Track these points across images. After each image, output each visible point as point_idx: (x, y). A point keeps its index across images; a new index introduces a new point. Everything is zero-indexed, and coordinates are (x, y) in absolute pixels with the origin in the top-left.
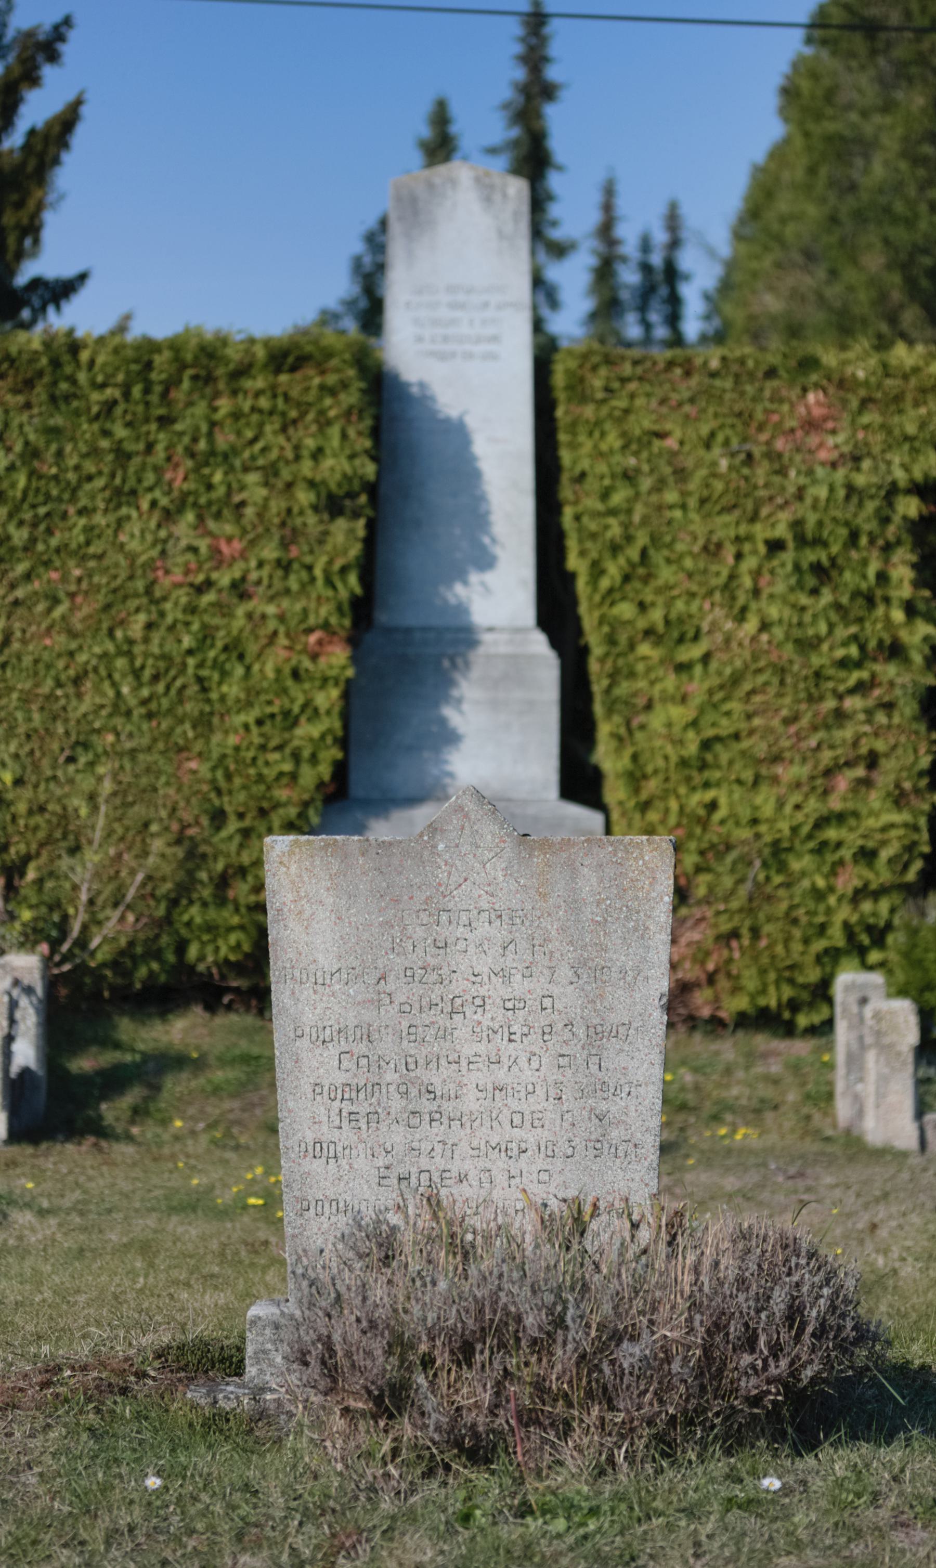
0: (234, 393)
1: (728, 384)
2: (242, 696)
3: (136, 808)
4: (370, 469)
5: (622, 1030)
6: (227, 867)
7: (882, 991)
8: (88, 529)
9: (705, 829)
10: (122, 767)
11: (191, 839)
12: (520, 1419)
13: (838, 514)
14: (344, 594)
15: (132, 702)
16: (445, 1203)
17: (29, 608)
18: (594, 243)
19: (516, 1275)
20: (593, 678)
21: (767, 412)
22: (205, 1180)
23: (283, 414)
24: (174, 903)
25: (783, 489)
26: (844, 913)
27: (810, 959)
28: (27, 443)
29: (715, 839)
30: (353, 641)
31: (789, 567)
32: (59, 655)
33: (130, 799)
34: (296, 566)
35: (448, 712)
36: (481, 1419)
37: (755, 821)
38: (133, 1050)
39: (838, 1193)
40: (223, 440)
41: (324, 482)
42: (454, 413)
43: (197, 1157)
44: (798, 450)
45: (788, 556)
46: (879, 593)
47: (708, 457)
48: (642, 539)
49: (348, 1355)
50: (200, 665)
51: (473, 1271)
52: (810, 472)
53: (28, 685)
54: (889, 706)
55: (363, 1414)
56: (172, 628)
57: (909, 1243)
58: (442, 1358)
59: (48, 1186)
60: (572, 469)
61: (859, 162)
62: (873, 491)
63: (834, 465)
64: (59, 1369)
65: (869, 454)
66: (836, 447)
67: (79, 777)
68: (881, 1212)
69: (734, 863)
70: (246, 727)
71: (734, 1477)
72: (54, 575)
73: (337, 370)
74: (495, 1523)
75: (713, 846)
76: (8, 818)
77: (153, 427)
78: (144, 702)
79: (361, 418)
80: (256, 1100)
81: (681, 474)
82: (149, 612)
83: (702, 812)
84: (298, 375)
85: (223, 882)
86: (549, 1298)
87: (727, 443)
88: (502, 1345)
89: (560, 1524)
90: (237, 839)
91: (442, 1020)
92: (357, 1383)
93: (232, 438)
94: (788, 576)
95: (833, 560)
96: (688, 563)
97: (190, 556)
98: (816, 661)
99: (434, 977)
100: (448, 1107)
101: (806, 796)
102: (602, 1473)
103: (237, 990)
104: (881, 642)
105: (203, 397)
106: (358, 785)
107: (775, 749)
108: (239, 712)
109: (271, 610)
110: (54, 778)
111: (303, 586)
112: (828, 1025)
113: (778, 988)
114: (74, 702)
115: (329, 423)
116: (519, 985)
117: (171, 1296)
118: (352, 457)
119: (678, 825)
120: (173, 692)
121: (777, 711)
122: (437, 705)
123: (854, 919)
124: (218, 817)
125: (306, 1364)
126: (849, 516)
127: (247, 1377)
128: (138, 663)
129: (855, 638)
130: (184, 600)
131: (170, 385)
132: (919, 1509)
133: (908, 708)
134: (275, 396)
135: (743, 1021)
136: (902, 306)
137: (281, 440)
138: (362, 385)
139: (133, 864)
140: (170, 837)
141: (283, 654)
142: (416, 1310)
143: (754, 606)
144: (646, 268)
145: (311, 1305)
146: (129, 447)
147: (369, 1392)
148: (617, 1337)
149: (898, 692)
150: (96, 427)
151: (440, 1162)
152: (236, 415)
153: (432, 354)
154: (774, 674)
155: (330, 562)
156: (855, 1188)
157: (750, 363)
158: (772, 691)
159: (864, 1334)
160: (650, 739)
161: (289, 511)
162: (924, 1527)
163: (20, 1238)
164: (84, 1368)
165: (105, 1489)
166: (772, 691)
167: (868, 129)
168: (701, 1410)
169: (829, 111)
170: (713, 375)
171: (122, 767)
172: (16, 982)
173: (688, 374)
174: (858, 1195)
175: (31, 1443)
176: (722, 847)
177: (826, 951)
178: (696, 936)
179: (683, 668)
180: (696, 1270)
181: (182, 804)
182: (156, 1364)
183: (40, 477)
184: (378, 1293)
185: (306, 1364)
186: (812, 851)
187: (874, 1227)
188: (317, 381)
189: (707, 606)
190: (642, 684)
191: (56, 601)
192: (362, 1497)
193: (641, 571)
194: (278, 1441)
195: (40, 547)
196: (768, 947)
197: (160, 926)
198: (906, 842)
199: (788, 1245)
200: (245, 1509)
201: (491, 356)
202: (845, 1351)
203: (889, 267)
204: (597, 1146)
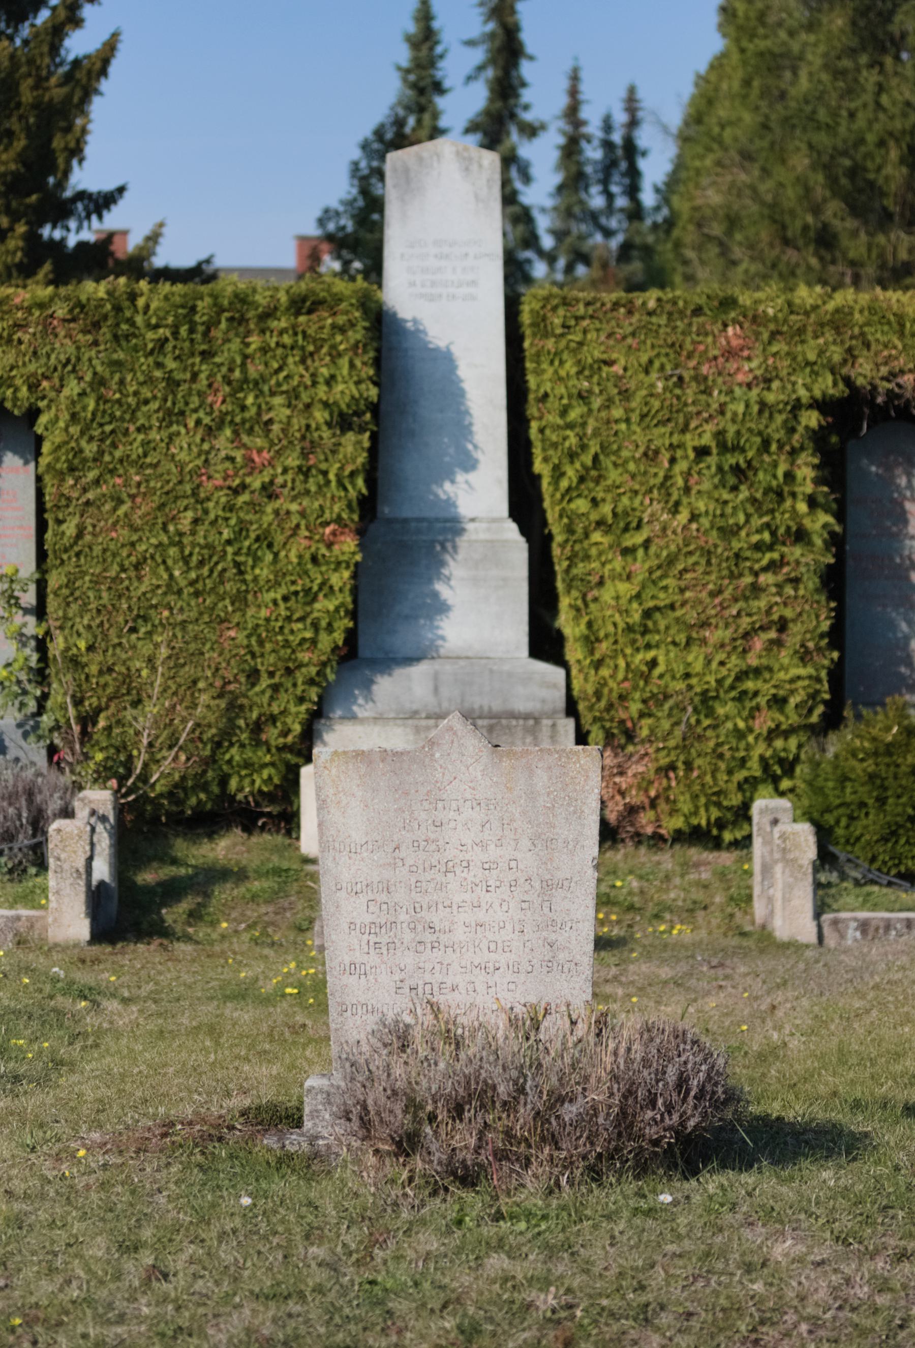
0: (263, 331)
1: (663, 320)
2: (272, 577)
3: (187, 668)
4: (373, 392)
5: (566, 883)
6: (260, 716)
7: (790, 815)
9: (647, 682)
10: (174, 635)
11: (231, 692)
12: (495, 1155)
13: (753, 426)
14: (353, 494)
15: (183, 583)
16: (442, 1007)
17: (99, 508)
18: (562, 124)
19: (492, 1058)
20: (556, 560)
21: (693, 342)
22: (250, 973)
23: (303, 348)
24: (219, 745)
25: (708, 405)
26: (760, 749)
27: (733, 786)
28: (95, 374)
29: (655, 690)
30: (361, 532)
31: (713, 469)
32: (123, 546)
33: (182, 661)
34: (314, 472)
35: (439, 587)
36: (469, 1156)
37: (687, 676)
38: (188, 866)
39: (749, 980)
40: (253, 371)
41: (336, 403)
42: (442, 344)
43: (242, 954)
44: (720, 374)
45: (712, 460)
46: (786, 489)
47: (647, 380)
48: (594, 447)
49: (378, 1113)
50: (236, 553)
51: (462, 1055)
52: (730, 392)
53: (98, 570)
54: (795, 581)
55: (389, 1153)
56: (213, 523)
57: (798, 1022)
59: (125, 979)
60: (537, 391)
61: (788, 74)
62: (781, 406)
63: (749, 386)
64: (172, 1124)
65: (777, 376)
66: (751, 370)
67: (140, 643)
68: (779, 996)
69: (671, 709)
70: (275, 602)
72: (119, 481)
73: (347, 312)
74: (479, 1226)
75: (653, 696)
76: (83, 677)
77: (198, 360)
78: (192, 583)
79: (365, 351)
80: (286, 905)
81: (626, 395)
82: (196, 510)
83: (644, 668)
84: (314, 317)
85: (257, 728)
86: (514, 1074)
87: (662, 368)
88: (483, 1106)
89: (523, 1226)
90: (268, 693)
91: (440, 877)
92: (384, 1132)
93: (261, 368)
94: (713, 477)
95: (749, 463)
96: (632, 466)
97: (228, 464)
98: (736, 545)
99: (433, 847)
100: (444, 938)
101: (729, 655)
102: (551, 1192)
103: (269, 815)
104: (788, 528)
105: (237, 335)
106: (364, 651)
107: (703, 616)
108: (268, 591)
109: (294, 507)
110: (120, 644)
111: (320, 487)
112: (746, 842)
113: (707, 810)
114: (136, 584)
115: (340, 355)
116: (493, 852)
118: (358, 383)
119: (626, 679)
120: (215, 574)
121: (704, 585)
122: (430, 581)
123: (768, 753)
124: (253, 676)
125: (349, 1120)
126: (762, 427)
127: (305, 1129)
128: (187, 552)
129: (767, 526)
130: (223, 500)
131: (209, 326)
132: (762, 1214)
133: (811, 582)
134: (296, 334)
135: (679, 837)
136: (825, 200)
137: (301, 369)
138: (367, 324)
139: (184, 713)
140: (214, 692)
141: (305, 543)
142: (424, 1083)
143: (685, 500)
144: (608, 145)
145: (353, 1079)
146: (178, 376)
147: (393, 1139)
148: (561, 1100)
149: (803, 569)
150: (151, 360)
151: (438, 977)
152: (264, 350)
153: (422, 296)
154: (702, 555)
155: (342, 468)
156: (763, 976)
157: (681, 304)
158: (700, 569)
159: (732, 1097)
160: (602, 610)
161: (308, 427)
162: (764, 1225)
163: (111, 1023)
164: (190, 1123)
165: (213, 1205)
166: (700, 569)
167: (795, 47)
169: (761, 31)
170: (650, 314)
171: (174, 635)
172: (93, 813)
173: (630, 312)
174: (764, 982)
176: (661, 697)
177: (746, 780)
178: (641, 769)
179: (627, 552)
180: (615, 1053)
181: (224, 665)
182: (241, 1120)
183: (106, 402)
184: (398, 1071)
185: (349, 1120)
186: (733, 699)
187: (774, 1007)
188: (330, 321)
189: (647, 501)
190: (595, 565)
191: (120, 502)
192: (389, 1210)
193: (594, 473)
195: (107, 458)
196: (699, 777)
197: (207, 764)
198: (811, 691)
200: (310, 1218)
201: (473, 298)
202: (717, 1108)
203: (813, 167)
204: (549, 965)
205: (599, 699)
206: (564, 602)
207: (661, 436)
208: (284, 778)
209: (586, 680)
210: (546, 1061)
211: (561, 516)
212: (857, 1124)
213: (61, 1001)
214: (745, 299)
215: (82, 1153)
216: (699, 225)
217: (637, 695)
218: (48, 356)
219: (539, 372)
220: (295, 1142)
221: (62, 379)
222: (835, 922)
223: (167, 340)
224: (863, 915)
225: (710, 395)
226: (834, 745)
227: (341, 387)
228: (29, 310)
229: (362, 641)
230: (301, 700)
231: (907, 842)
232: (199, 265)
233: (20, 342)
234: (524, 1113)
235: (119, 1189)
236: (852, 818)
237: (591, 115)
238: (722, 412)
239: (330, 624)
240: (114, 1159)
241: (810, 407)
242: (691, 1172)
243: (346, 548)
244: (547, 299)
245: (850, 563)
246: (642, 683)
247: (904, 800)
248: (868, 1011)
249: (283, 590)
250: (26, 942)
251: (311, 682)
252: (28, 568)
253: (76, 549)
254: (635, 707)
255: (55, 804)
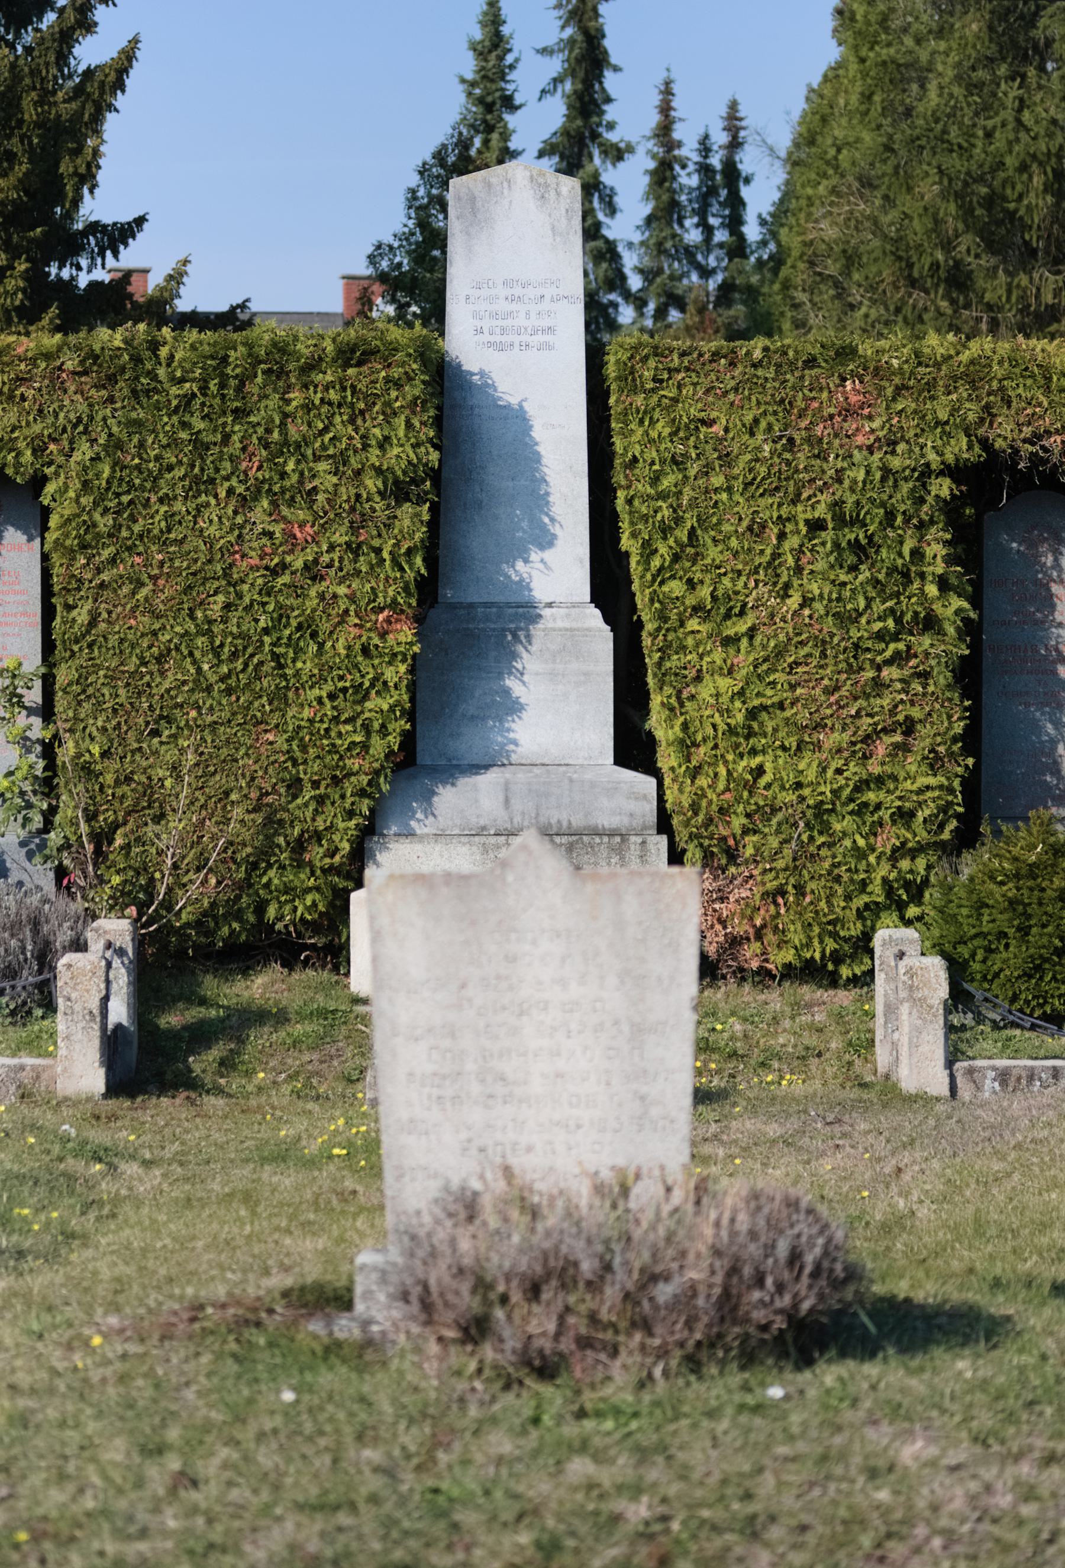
0: (306, 386)
1: (771, 374)
8: (169, 516)
14: (410, 575)
15: (212, 679)
21: (805, 399)
22: (292, 1132)
23: (352, 405)
24: (255, 866)
26: (883, 870)
27: (851, 915)
30: (419, 620)
35: (510, 682)
37: (799, 785)
39: (870, 1138)
40: (294, 432)
42: (514, 401)
43: (282, 1109)
44: (836, 435)
45: (828, 535)
50: (273, 644)
54: (924, 676)
56: (248, 609)
58: (516, 1297)
59: (147, 1138)
62: (907, 472)
64: (202, 1307)
68: (906, 1158)
69: (779, 824)
71: (746, 1388)
72: (138, 560)
73: (403, 364)
78: (222, 680)
79: (424, 410)
80: (333, 1051)
81: (727, 459)
85: (299, 846)
86: (600, 1248)
87: (770, 428)
88: (563, 1286)
89: (609, 1424)
92: (449, 1316)
96: (734, 543)
97: (264, 540)
106: (424, 757)
109: (342, 590)
113: (821, 942)
117: (276, 1242)
119: (728, 789)
122: (500, 676)
123: (893, 876)
124: (295, 786)
129: (892, 611)
130: (260, 581)
133: (942, 677)
134: (344, 389)
135: (789, 973)
141: (355, 631)
142: (495, 1259)
143: (796, 583)
144: (705, 169)
148: (654, 1278)
150: (175, 419)
152: (307, 407)
155: (397, 545)
159: (853, 1274)
161: (358, 496)
163: (130, 1189)
164: (223, 1306)
165: (251, 1401)
168: (720, 1336)
172: (109, 945)
175: (186, 1367)
177: (867, 906)
179: (729, 642)
180: (717, 1224)
184: (465, 1245)
193: (690, 550)
194: (384, 1364)
195: (125, 533)
197: (241, 888)
199: (792, 1204)
200: (363, 1416)
201: (549, 347)
203: (944, 195)
205: (696, 814)
206: (656, 701)
207: (768, 508)
208: (331, 905)
209: (681, 791)
210: (637, 1234)
211: (652, 601)
212: (999, 1306)
213: (71, 1164)
214: (866, 348)
215: (97, 1341)
216: (812, 264)
217: (740, 809)
218: (56, 415)
219: (626, 434)
220: (345, 1327)
221: (71, 442)
222: (970, 1071)
223: (194, 395)
224: (1003, 1063)
225: (826, 460)
226: (969, 866)
227: (396, 451)
228: (33, 361)
229: (420, 746)
230: (350, 814)
231: (1054, 978)
232: (233, 309)
233: (23, 398)
234: (612, 1293)
235: (140, 1382)
236: (989, 950)
237: (687, 135)
238: (839, 481)
239: (383, 726)
240: (133, 1348)
241: (941, 473)
242: (805, 1361)
243: (402, 638)
244: (636, 348)
245: (988, 655)
246: (746, 794)
247: (1050, 929)
248: (1009, 1175)
249: (329, 687)
250: (30, 1095)
251: (362, 793)
252: (33, 662)
253: (89, 639)
254: (738, 822)
255: (64, 936)
